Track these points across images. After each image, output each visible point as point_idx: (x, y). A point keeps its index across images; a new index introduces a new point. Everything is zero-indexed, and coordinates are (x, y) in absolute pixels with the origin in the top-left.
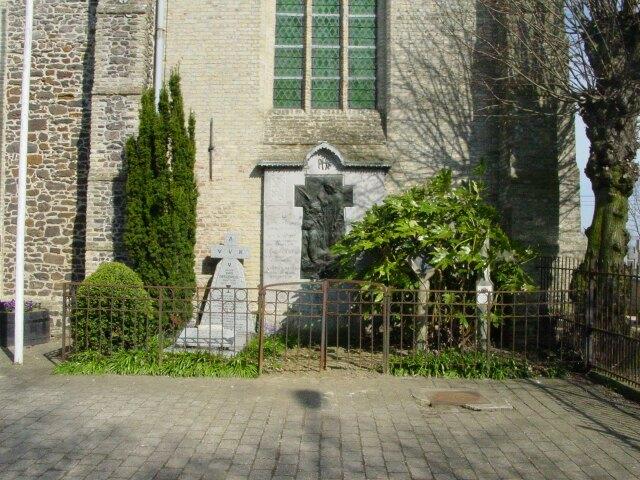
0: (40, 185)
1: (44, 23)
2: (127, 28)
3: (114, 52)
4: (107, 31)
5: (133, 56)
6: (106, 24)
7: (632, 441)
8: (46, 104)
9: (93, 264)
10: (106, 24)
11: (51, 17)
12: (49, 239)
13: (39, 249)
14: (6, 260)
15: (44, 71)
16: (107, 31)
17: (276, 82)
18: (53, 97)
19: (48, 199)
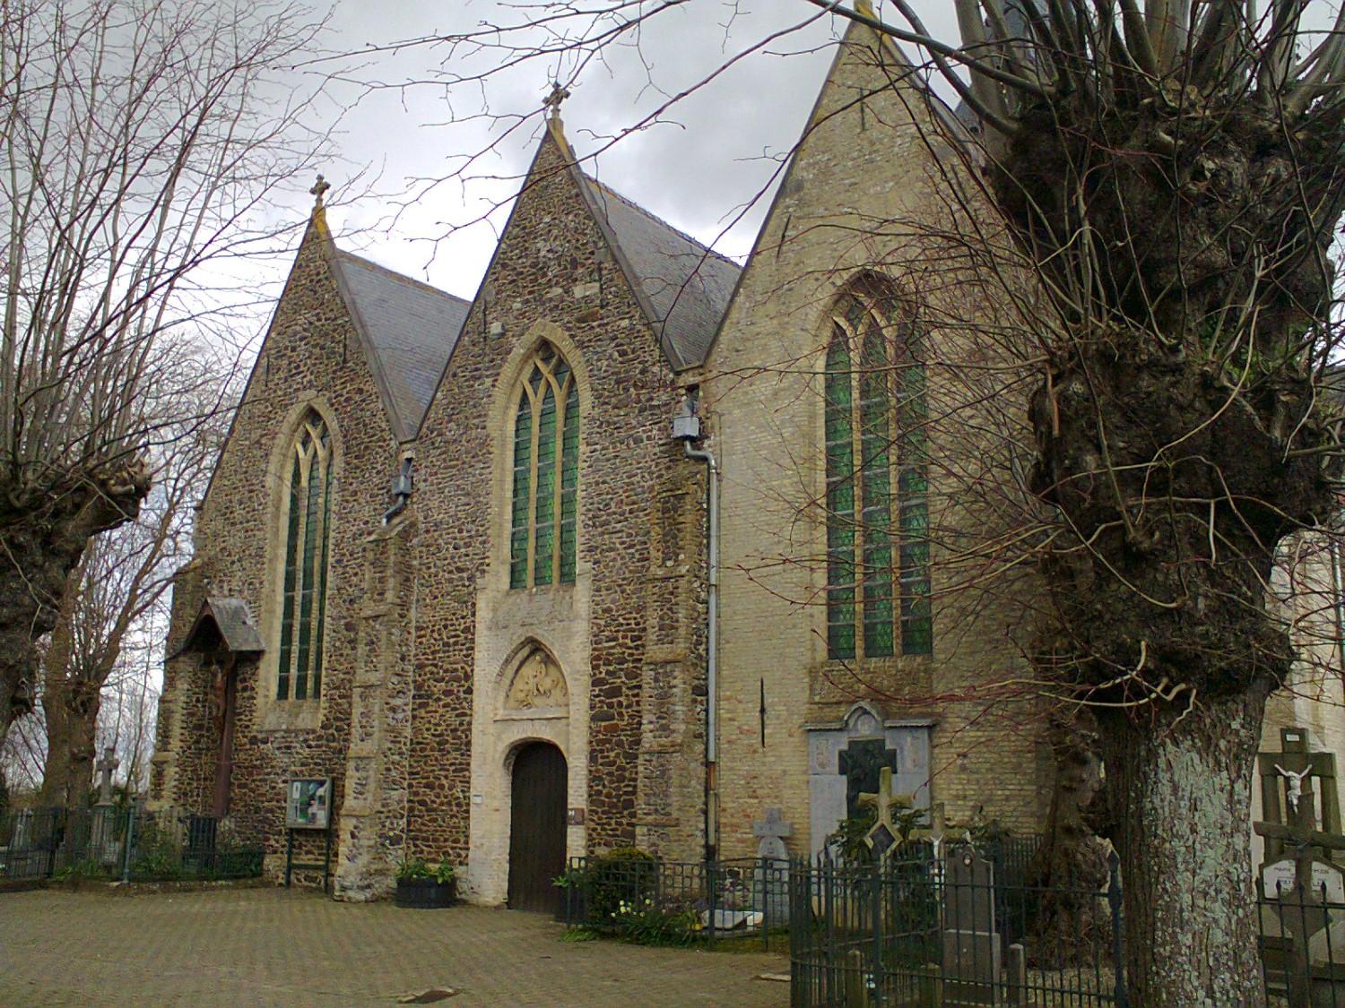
0: (617, 755)
1: (620, 586)
2: (672, 593)
3: (661, 618)
4: (655, 597)
5: (677, 621)
6: (655, 590)
7: (932, 99)
8: (621, 670)
9: (1245, 5)
10: (655, 590)
11: (624, 579)
12: (626, 813)
13: (617, 823)
14: (590, 835)
15: (620, 634)
16: (655, 597)
17: (829, 627)
18: (627, 661)
19: (624, 769)
